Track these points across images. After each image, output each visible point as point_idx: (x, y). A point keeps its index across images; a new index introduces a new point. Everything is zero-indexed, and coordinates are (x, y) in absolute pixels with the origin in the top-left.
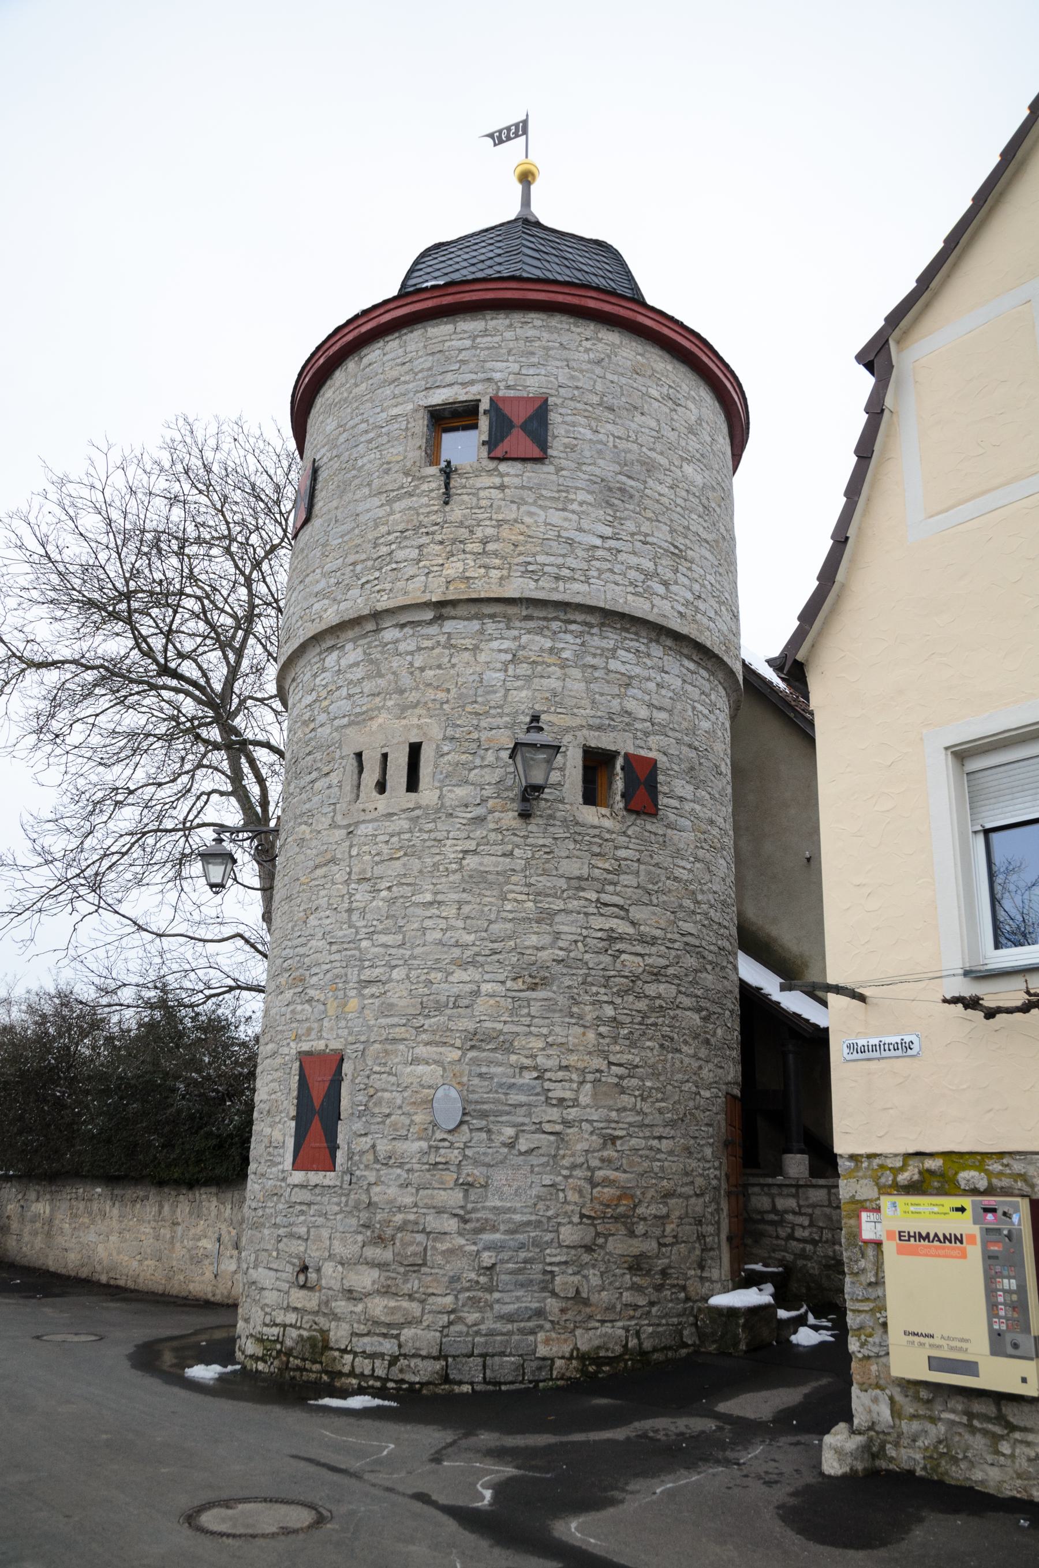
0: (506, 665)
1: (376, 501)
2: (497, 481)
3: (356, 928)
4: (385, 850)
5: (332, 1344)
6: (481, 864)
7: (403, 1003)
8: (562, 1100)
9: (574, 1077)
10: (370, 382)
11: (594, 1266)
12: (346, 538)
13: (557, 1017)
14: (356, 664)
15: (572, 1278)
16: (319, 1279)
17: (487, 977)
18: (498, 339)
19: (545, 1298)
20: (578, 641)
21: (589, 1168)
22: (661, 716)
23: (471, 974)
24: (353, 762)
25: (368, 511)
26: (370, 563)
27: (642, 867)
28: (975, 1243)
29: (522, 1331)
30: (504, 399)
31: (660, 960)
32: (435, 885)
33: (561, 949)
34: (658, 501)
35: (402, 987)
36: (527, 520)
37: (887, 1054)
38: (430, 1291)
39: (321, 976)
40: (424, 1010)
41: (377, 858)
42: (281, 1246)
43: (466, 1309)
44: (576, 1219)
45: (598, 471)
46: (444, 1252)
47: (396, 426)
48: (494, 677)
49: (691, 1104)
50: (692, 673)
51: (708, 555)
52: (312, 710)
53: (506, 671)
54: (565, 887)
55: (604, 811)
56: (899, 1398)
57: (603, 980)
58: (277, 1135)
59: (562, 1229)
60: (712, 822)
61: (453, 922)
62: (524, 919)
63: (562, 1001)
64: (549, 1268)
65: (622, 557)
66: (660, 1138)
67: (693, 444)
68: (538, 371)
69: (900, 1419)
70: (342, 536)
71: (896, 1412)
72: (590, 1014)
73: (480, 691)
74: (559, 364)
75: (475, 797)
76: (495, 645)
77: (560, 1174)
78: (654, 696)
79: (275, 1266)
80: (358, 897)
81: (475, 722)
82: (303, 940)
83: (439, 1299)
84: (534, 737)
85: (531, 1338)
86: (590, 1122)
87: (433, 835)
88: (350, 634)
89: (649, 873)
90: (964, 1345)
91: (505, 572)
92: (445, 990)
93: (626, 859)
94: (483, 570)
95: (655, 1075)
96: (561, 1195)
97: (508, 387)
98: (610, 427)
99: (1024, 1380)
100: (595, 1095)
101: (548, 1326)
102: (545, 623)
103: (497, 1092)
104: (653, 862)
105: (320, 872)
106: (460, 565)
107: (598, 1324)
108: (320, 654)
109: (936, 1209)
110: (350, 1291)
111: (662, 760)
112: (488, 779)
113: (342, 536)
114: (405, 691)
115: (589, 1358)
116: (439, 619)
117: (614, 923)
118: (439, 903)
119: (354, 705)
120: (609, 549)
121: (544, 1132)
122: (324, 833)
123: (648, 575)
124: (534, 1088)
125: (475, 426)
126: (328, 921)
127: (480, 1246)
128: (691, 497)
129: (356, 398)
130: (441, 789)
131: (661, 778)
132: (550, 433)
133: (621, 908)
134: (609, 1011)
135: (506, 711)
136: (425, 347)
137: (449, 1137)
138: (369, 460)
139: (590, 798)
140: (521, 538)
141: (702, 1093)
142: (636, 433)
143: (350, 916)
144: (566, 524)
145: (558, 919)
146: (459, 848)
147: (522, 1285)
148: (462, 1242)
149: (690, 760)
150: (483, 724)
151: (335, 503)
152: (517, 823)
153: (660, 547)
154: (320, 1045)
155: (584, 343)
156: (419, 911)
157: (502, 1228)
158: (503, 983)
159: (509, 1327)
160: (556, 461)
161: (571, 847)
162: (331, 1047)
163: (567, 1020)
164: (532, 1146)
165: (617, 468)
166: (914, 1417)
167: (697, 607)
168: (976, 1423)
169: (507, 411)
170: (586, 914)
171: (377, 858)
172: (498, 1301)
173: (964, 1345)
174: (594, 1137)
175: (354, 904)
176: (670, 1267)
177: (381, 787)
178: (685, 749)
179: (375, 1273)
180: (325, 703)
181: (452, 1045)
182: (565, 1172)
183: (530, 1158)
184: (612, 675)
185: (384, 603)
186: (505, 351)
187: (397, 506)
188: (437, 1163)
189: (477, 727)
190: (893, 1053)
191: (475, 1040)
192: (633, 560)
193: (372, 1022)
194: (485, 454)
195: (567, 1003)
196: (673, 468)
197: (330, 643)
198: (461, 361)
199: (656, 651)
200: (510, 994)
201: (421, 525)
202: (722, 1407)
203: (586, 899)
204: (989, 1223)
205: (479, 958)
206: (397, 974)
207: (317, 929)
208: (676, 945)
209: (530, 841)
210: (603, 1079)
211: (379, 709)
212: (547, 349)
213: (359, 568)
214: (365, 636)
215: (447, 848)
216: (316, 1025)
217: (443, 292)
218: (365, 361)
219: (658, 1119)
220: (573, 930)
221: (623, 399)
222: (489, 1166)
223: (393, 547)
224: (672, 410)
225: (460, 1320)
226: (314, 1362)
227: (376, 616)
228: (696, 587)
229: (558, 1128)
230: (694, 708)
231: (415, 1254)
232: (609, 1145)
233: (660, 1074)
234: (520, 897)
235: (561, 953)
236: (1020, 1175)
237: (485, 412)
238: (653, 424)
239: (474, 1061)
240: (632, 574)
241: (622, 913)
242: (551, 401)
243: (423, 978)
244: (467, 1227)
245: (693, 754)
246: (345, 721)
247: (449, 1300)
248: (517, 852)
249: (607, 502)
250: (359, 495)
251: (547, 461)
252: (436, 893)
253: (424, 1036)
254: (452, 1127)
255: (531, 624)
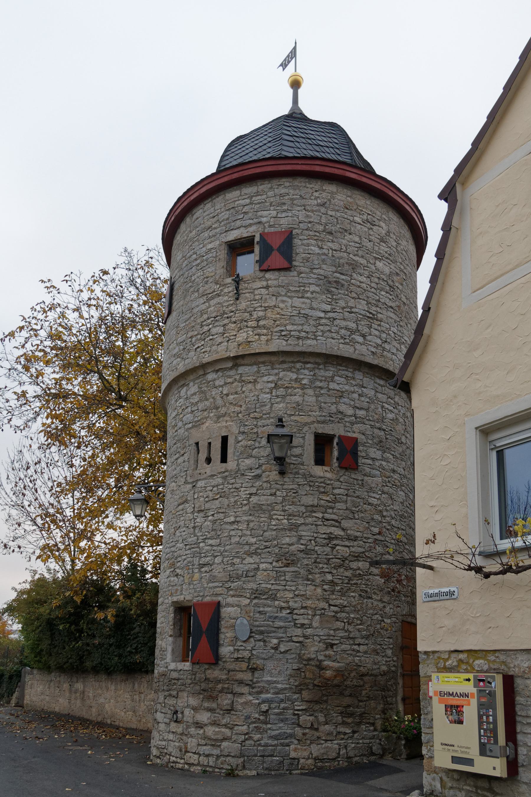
0: (271, 389)
1: (202, 300)
2: (264, 283)
3: (197, 536)
4: (211, 494)
5: (188, 750)
6: (259, 500)
7: (220, 575)
8: (303, 625)
9: (310, 612)
10: (197, 229)
11: (321, 711)
12: (187, 323)
13: (300, 581)
14: (195, 394)
15: (309, 718)
16: (183, 717)
17: (262, 560)
18: (264, 197)
19: (295, 728)
20: (312, 373)
21: (318, 660)
22: (361, 413)
23: (256, 559)
24: (194, 447)
25: (198, 306)
26: (199, 337)
27: (349, 498)
28: (474, 698)
29: (282, 745)
30: (268, 233)
31: (360, 549)
32: (235, 512)
33: (302, 544)
34: (359, 287)
35: (220, 567)
36: (282, 305)
37: (442, 598)
38: (235, 723)
39: (182, 562)
40: (231, 579)
41: (207, 499)
42: (166, 701)
43: (254, 732)
44: (311, 687)
45: (322, 272)
46: (242, 703)
47: (211, 255)
48: (265, 397)
49: (378, 626)
50: (382, 386)
51: (392, 315)
52: (176, 420)
53: (271, 393)
54: (304, 511)
55: (326, 468)
56: (445, 778)
57: (326, 561)
58: (164, 645)
59: (303, 692)
60: (394, 471)
61: (244, 532)
62: (282, 529)
63: (303, 572)
64: (296, 712)
65: (336, 322)
66: (359, 645)
67: (383, 248)
68: (287, 214)
69: (445, 789)
70: (185, 322)
71: (443, 786)
72: (318, 578)
73: (258, 406)
74: (299, 208)
75: (255, 464)
76: (265, 379)
77: (302, 663)
78: (357, 401)
79: (163, 711)
80: (198, 520)
81: (255, 423)
82: (173, 544)
83: (240, 727)
84: (280, 431)
85: (287, 748)
86: (319, 636)
87: (234, 486)
88: (192, 377)
89: (353, 501)
90: (468, 750)
91: (269, 337)
92: (242, 568)
93: (339, 494)
94: (257, 337)
95: (356, 611)
96: (303, 674)
97: (270, 226)
98: (330, 244)
99: (494, 768)
100: (321, 622)
101: (296, 742)
102: (293, 365)
103: (268, 621)
104: (355, 495)
105: (181, 507)
106: (245, 334)
107: (323, 742)
108: (178, 389)
109: (457, 680)
110: (197, 723)
111: (361, 438)
112: (262, 454)
113: (185, 322)
114: (219, 407)
115: (318, 759)
116: (236, 366)
117: (332, 530)
118: (238, 522)
119: (195, 417)
120: (329, 319)
121: (293, 642)
122: (182, 486)
123: (352, 332)
124: (287, 618)
125: (252, 252)
126: (184, 533)
127: (260, 701)
128: (381, 282)
129: (191, 240)
130: (238, 460)
131: (360, 448)
132: (294, 252)
133: (336, 521)
134: (329, 577)
135: (272, 416)
136: (225, 206)
137: (244, 644)
138: (198, 276)
139: (320, 461)
140: (278, 316)
141: (385, 620)
142: (346, 246)
143: (194, 531)
144: (303, 306)
145: (300, 528)
146: (248, 492)
147: (282, 721)
148: (251, 698)
149: (379, 437)
150: (259, 424)
151: (181, 303)
152: (278, 477)
153: (360, 314)
154: (181, 598)
155: (315, 194)
156: (228, 527)
157: (272, 691)
158: (271, 563)
159: (276, 742)
160: (298, 269)
161: (308, 489)
162: (186, 599)
163: (306, 582)
164: (287, 649)
165: (334, 269)
166: (451, 788)
167: (384, 348)
168: (479, 791)
169: (269, 241)
170: (316, 525)
171: (207, 499)
172: (270, 729)
173: (468, 750)
174: (321, 644)
175: (196, 524)
176: (365, 713)
177: (209, 460)
178: (376, 431)
179: (209, 714)
180: (181, 416)
181: (245, 597)
182: (304, 662)
183: (286, 655)
184: (331, 392)
185: (207, 359)
186: (268, 204)
187: (212, 302)
188: (238, 658)
189: (256, 426)
190: (445, 597)
191: (257, 594)
192: (343, 323)
193: (205, 586)
194: (257, 268)
195: (306, 573)
196: (369, 265)
197: (182, 383)
198: (244, 212)
199: (359, 375)
200: (275, 569)
201: (224, 313)
202: (370, 783)
203: (316, 517)
204: (481, 687)
205: (259, 551)
206: (218, 560)
207: (180, 538)
208: (369, 541)
209: (285, 487)
210: (326, 613)
211: (206, 418)
212: (292, 200)
213: (194, 339)
214: (198, 378)
215: (242, 492)
216: (179, 588)
217: (247, 168)
218: (195, 217)
219: (357, 634)
220: (309, 534)
221: (338, 226)
222: (265, 659)
223: (210, 326)
224: (369, 229)
225: (250, 738)
226: (181, 759)
227: (204, 366)
228: (384, 336)
229: (301, 639)
230: (383, 407)
231: (227, 705)
232: (330, 649)
233: (359, 611)
234: (280, 517)
235: (302, 547)
236: (503, 662)
237: (258, 243)
238: (357, 239)
239: (256, 605)
240: (343, 332)
241: (337, 524)
242: (294, 232)
243: (230, 562)
244: (254, 690)
245: (382, 433)
246: (190, 425)
247: (245, 727)
248: (278, 493)
249: (328, 290)
250: (193, 297)
251: (292, 269)
252: (236, 517)
253: (231, 592)
254: (245, 639)
255: (285, 366)
